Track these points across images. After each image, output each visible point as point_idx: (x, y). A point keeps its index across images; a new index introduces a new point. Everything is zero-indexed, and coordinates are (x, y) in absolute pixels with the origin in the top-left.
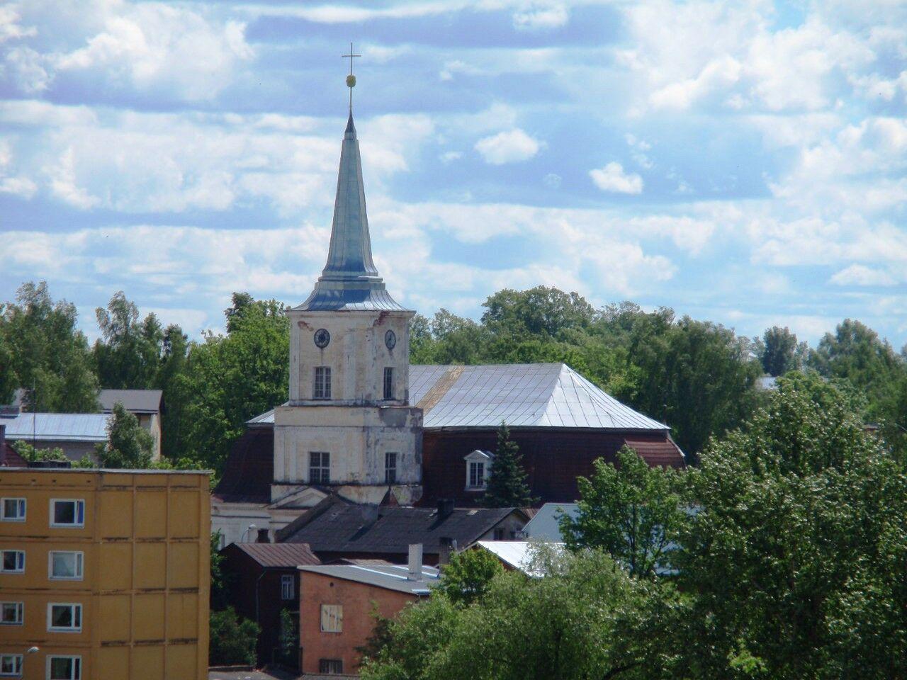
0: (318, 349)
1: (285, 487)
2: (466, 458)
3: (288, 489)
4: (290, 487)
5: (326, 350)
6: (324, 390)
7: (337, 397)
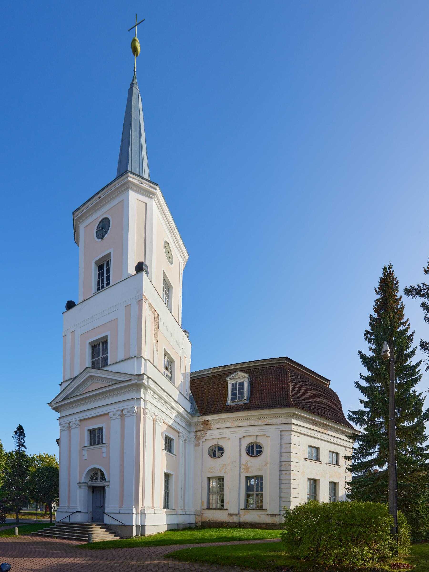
2: (228, 379)
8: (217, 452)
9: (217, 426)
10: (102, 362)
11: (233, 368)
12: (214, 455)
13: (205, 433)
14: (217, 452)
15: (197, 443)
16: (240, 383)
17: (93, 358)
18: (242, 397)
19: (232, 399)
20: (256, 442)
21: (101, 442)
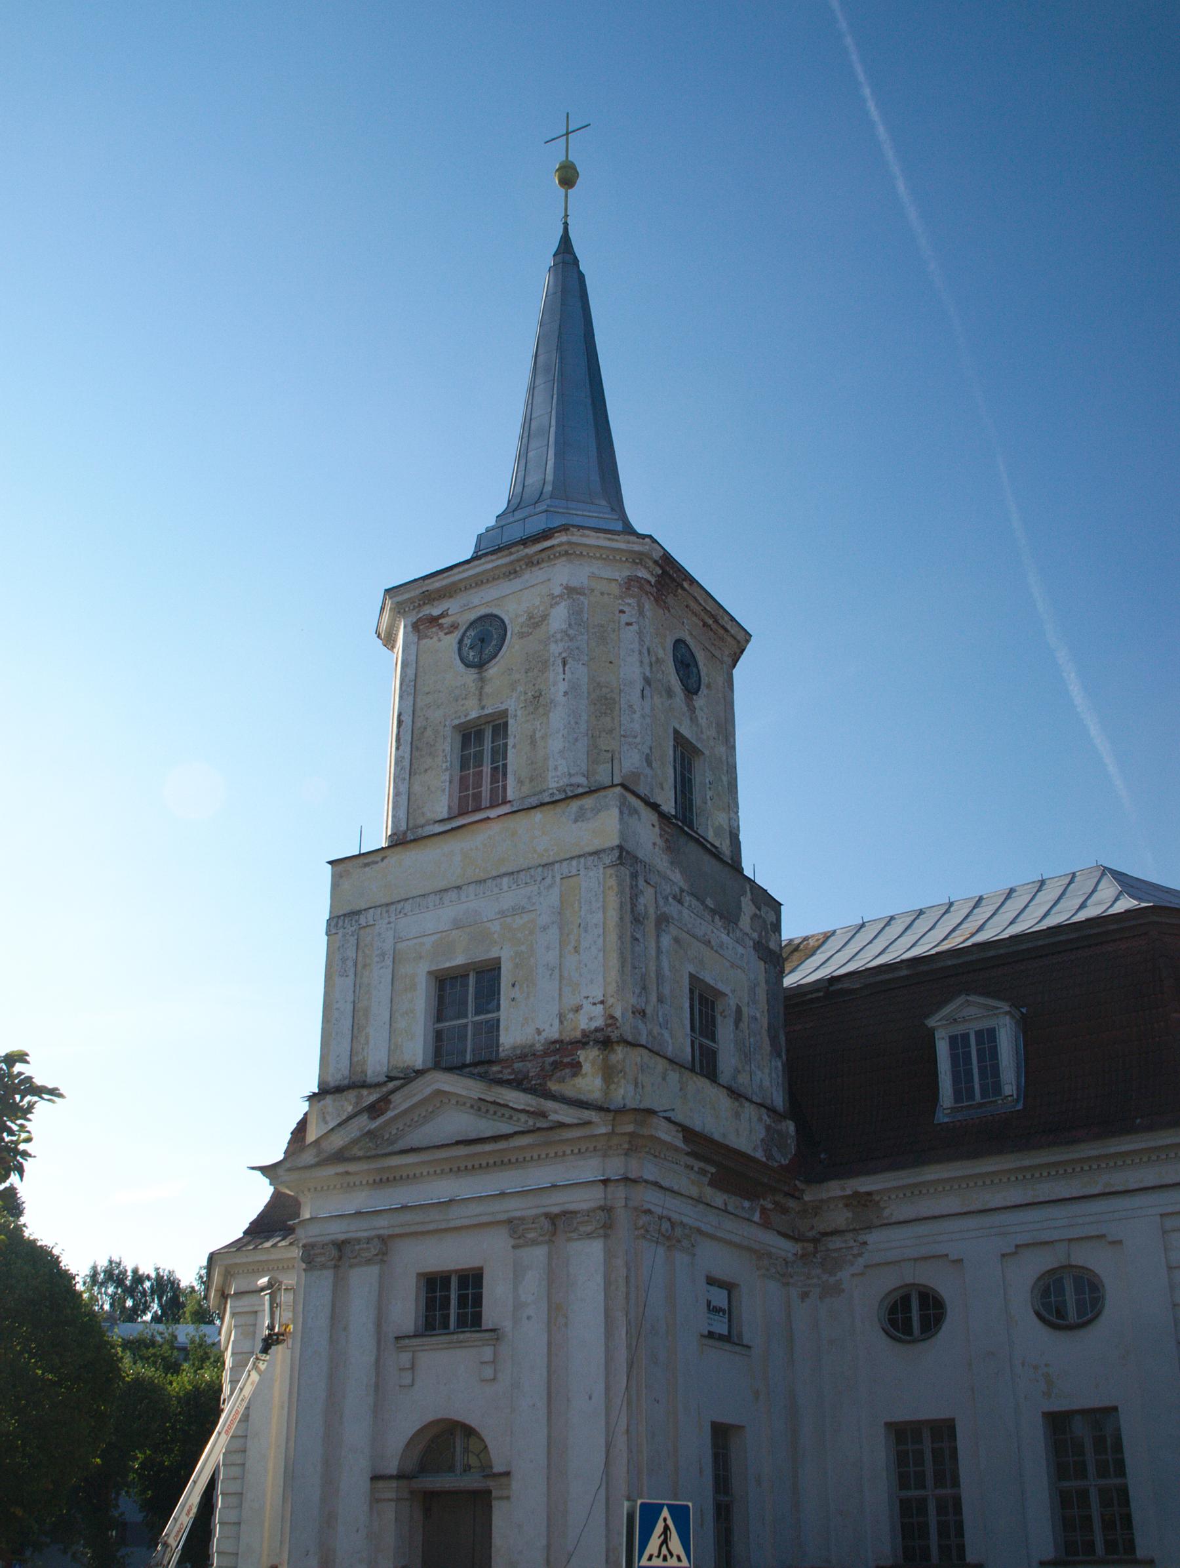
0: (470, 676)
1: (351, 1095)
2: (931, 1022)
4: (365, 1092)
5: (493, 670)
7: (526, 790)
8: (914, 1314)
9: (906, 1211)
10: (474, 1035)
11: (949, 963)
12: (907, 1329)
13: (861, 1238)
14: (914, 1314)
15: (832, 1280)
16: (979, 1034)
17: (440, 1017)
18: (997, 1088)
21: (471, 1318)
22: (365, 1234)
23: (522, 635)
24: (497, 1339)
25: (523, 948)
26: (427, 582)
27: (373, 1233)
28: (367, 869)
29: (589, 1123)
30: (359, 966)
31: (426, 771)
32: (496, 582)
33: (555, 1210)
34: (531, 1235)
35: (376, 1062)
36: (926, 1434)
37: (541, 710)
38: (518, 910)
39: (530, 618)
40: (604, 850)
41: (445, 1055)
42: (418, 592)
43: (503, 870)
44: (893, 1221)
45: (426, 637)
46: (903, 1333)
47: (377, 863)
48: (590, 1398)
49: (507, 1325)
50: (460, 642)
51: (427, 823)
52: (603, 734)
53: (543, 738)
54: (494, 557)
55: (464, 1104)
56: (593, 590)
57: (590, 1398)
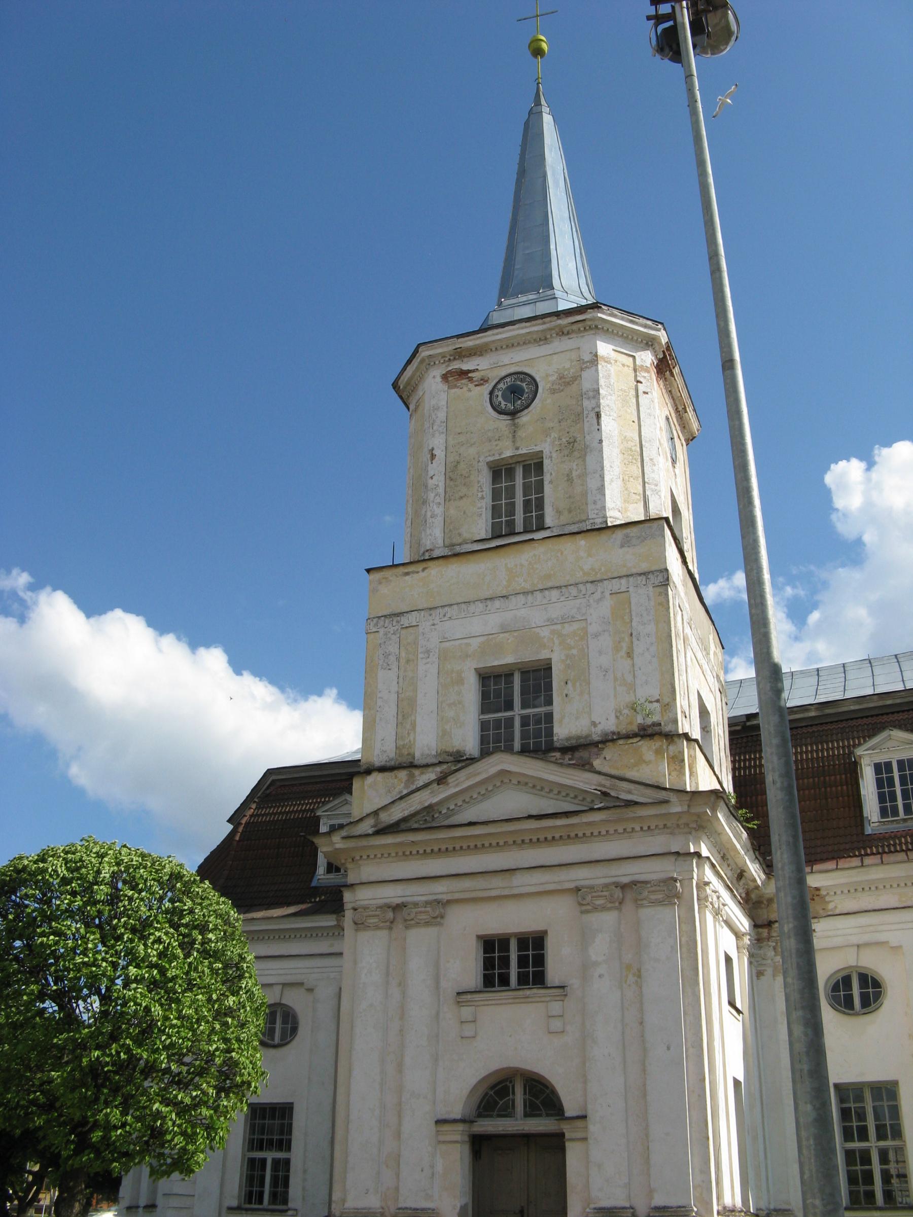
0: (503, 422)
1: (403, 774)
2: (859, 751)
3: (411, 777)
4: (416, 772)
5: (525, 418)
6: (278, 1026)
7: (565, 518)
11: (852, 708)
19: (884, 812)
20: (857, 966)
22: (424, 898)
23: (553, 391)
24: (566, 995)
25: (574, 652)
26: (460, 340)
27: (431, 898)
28: (407, 578)
29: (666, 802)
30: (403, 661)
31: (461, 498)
32: (525, 347)
33: (625, 880)
34: (599, 902)
35: (426, 742)
36: (868, 1095)
37: (576, 454)
38: (566, 620)
39: (561, 378)
40: (652, 572)
41: (493, 740)
42: (451, 348)
43: (550, 584)
44: (837, 912)
45: (456, 387)
46: (845, 1008)
47: (418, 572)
48: (668, 1048)
49: (574, 983)
50: (491, 393)
51: (465, 542)
52: (631, 479)
53: (579, 476)
54: (528, 324)
55: (526, 784)
56: (616, 361)
57: (668, 1048)
